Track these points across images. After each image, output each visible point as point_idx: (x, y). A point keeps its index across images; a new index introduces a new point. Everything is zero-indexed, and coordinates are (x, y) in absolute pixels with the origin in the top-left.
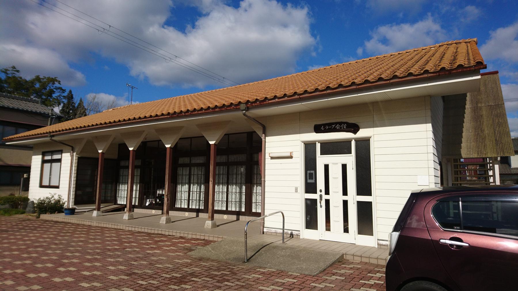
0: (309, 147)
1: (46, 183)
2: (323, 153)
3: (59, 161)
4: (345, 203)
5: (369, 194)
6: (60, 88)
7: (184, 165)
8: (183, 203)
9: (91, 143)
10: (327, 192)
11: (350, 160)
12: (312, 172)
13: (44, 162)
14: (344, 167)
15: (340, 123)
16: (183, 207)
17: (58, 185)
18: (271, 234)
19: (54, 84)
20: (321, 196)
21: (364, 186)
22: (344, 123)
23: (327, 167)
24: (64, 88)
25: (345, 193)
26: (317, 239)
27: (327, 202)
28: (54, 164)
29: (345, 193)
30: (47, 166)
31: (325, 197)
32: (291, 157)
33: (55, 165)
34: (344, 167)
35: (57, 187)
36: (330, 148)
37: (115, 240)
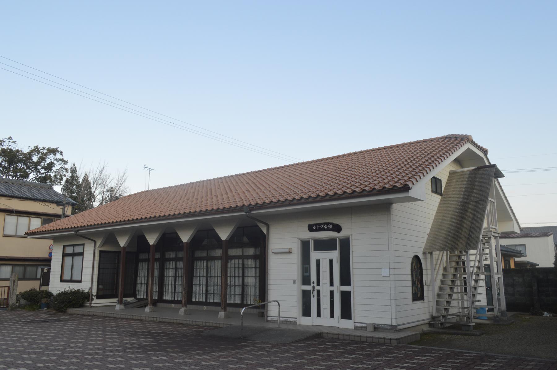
0: (305, 244)
1: (67, 277)
2: (316, 249)
3: (82, 254)
4: (332, 293)
5: (349, 284)
6: (62, 160)
7: (201, 259)
8: (236, 298)
9: (110, 238)
10: (318, 284)
11: (335, 255)
12: (307, 266)
13: (64, 255)
14: (331, 261)
15: (328, 224)
16: (236, 302)
17: (80, 279)
18: (274, 322)
19: (55, 155)
20: (314, 287)
21: (346, 279)
22: (331, 224)
23: (318, 262)
24: (66, 160)
25: (332, 284)
26: (310, 324)
27: (319, 292)
28: (76, 258)
29: (332, 284)
30: (68, 260)
31: (317, 288)
32: (290, 252)
33: (78, 259)
34: (331, 261)
35: (80, 281)
36: (322, 245)
37: (118, 351)
